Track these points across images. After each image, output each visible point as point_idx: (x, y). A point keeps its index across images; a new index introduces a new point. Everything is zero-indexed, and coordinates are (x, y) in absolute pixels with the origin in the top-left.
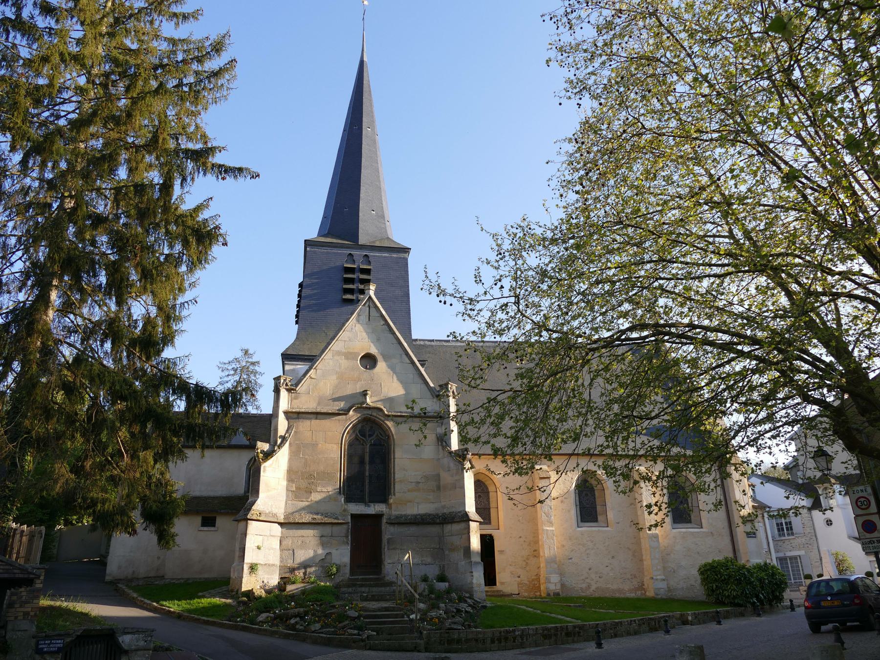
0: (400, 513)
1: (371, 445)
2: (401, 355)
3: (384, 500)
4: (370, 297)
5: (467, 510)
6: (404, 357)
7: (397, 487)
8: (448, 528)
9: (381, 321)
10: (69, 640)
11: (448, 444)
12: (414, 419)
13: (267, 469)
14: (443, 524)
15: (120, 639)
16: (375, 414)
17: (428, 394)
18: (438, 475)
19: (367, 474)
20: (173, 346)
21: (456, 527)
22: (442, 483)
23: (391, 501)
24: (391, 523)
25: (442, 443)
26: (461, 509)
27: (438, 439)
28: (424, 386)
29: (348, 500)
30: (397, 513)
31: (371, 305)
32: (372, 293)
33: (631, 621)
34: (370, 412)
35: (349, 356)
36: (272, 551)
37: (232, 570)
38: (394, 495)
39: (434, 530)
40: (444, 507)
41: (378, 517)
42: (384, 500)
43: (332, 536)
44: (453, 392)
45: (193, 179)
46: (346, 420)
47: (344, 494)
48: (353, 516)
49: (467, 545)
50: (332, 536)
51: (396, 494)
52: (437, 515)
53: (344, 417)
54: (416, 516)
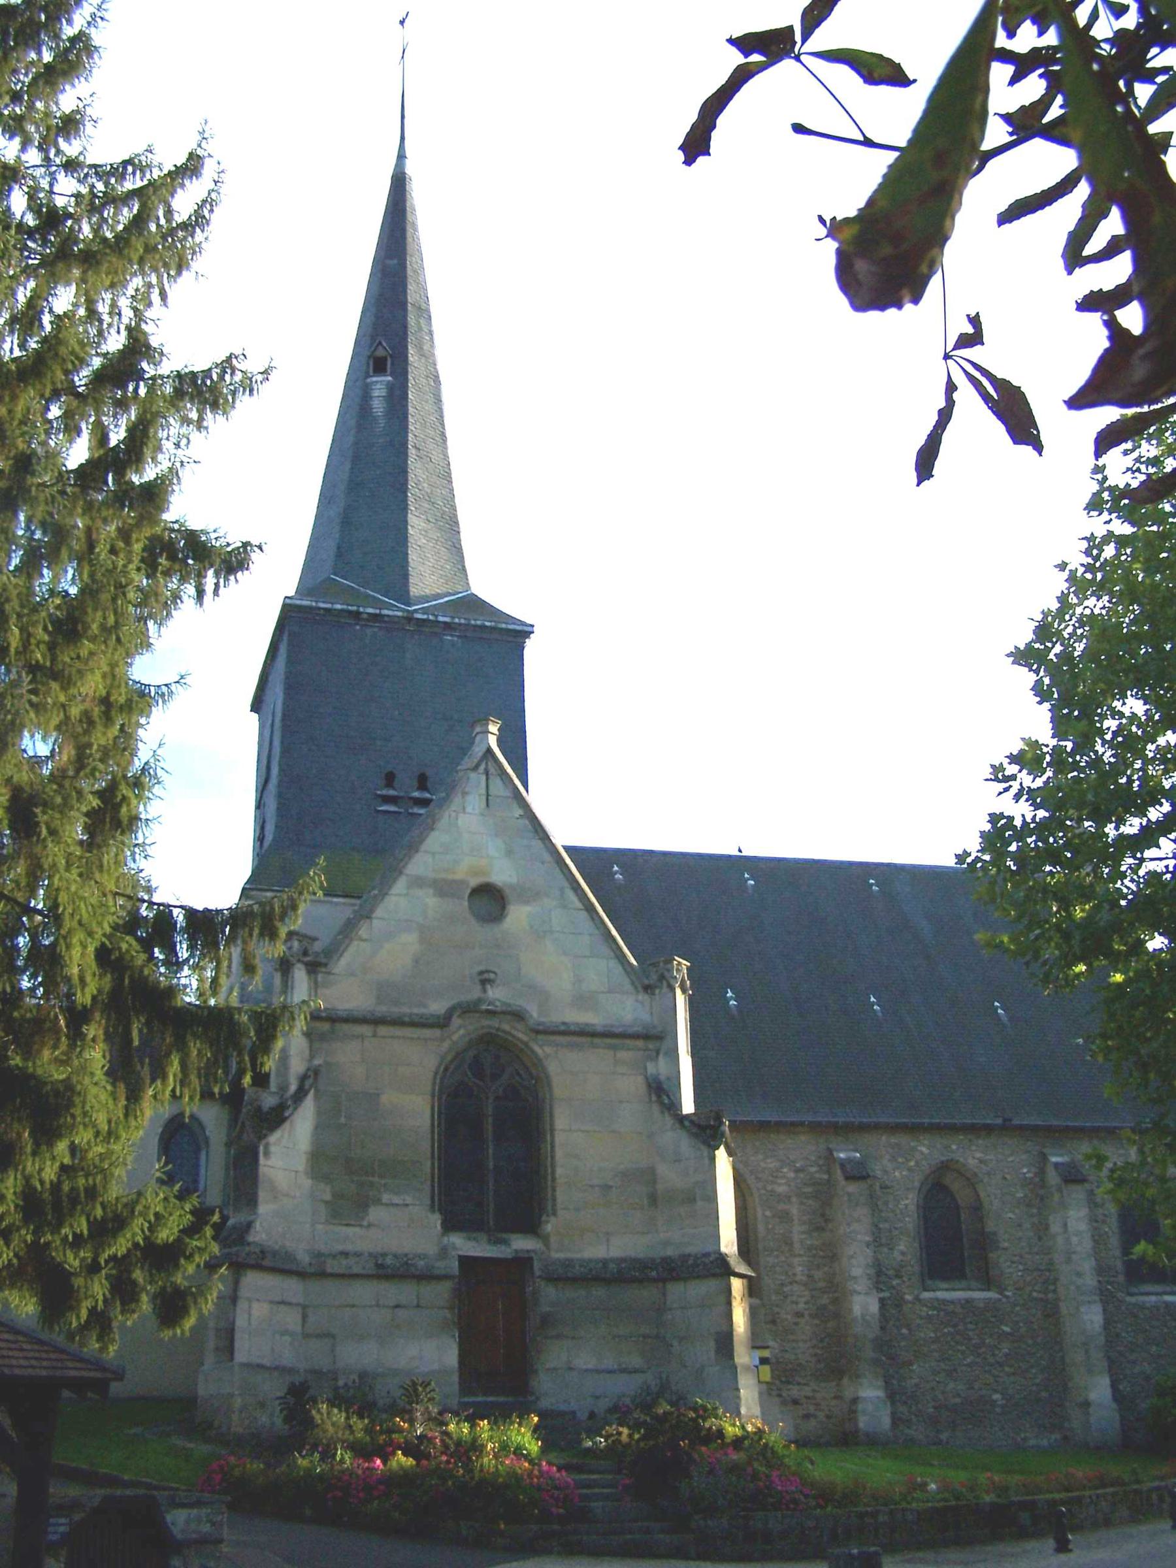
0: (569, 1255)
1: (497, 1098)
2: (562, 890)
3: (531, 1227)
4: (489, 751)
5: (723, 1249)
6: (571, 896)
7: (561, 1196)
8: (675, 1290)
9: (515, 805)
10: (77, 1517)
11: (673, 1106)
12: (597, 1041)
13: (273, 1149)
14: (664, 1281)
15: (169, 1518)
16: (506, 1027)
17: (626, 983)
18: (652, 1171)
19: (491, 1165)
20: (835, 228)
21: (697, 1290)
22: (660, 1187)
23: (549, 1228)
24: (553, 1278)
25: (659, 1097)
26: (709, 1248)
27: (649, 1086)
28: (614, 964)
29: (450, 1225)
30: (561, 1255)
31: (492, 770)
32: (493, 741)
33: (1098, 1496)
34: (494, 1023)
35: (444, 888)
36: (287, 1338)
37: (201, 1378)
38: (554, 1214)
39: (646, 1295)
40: (666, 1243)
41: (522, 1262)
42: (531, 1227)
43: (418, 1306)
44: (683, 981)
45: (163, 296)
46: (442, 1040)
47: (440, 1210)
48: (465, 1261)
49: (725, 1328)
50: (418, 1306)
51: (560, 1213)
52: (653, 1260)
53: (437, 1032)
54: (605, 1262)
